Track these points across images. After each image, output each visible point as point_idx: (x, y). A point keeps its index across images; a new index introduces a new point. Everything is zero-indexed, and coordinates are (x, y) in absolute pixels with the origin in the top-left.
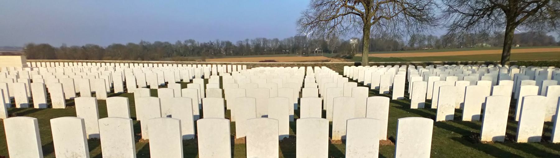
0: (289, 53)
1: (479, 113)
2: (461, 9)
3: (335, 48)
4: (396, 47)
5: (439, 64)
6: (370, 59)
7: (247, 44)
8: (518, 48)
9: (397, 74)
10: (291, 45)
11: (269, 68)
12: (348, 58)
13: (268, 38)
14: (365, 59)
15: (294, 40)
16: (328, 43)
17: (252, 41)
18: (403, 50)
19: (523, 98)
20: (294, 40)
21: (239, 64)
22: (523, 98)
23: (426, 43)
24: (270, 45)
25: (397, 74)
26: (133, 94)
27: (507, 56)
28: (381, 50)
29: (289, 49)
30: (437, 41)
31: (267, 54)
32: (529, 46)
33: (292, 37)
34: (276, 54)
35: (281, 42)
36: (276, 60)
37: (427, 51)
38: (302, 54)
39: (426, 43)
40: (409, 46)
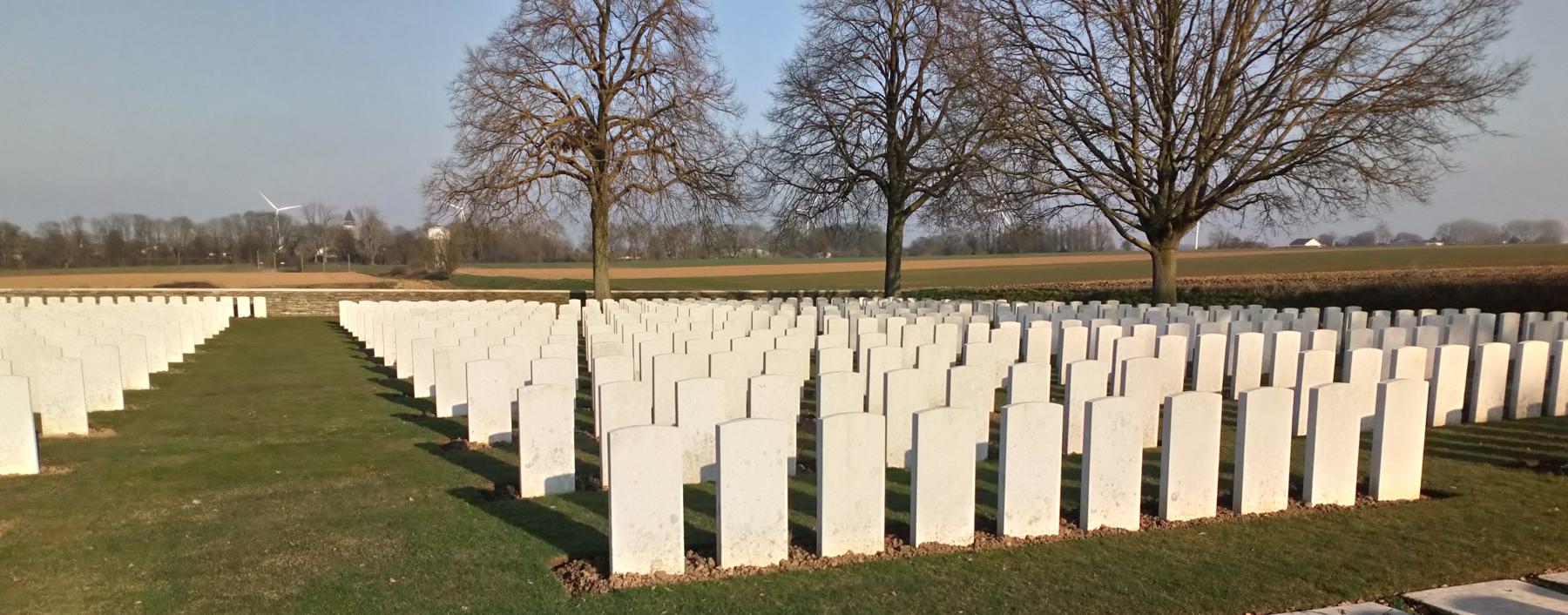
0: (230, 262)
1: (509, 429)
2: (796, 178)
3: (380, 249)
4: (554, 254)
5: (761, 295)
6: (615, 284)
7: (79, 235)
8: (828, 261)
9: (799, 313)
10: (235, 237)
11: (464, 303)
12: (432, 277)
13: (153, 214)
14: (603, 283)
15: (244, 222)
16: (357, 236)
17: (95, 222)
18: (569, 259)
19: (1069, 366)
20: (244, 222)
21: (243, 294)
22: (1069, 366)
23: (627, 244)
24: (163, 236)
25: (799, 313)
26: (151, 375)
27: (895, 279)
28: (512, 259)
29: (229, 249)
30: (653, 241)
31: (153, 263)
32: (798, 259)
33: (237, 216)
34: (184, 263)
35: (201, 229)
36: (214, 282)
37: (630, 264)
38: (278, 262)
39: (627, 244)
40: (584, 251)
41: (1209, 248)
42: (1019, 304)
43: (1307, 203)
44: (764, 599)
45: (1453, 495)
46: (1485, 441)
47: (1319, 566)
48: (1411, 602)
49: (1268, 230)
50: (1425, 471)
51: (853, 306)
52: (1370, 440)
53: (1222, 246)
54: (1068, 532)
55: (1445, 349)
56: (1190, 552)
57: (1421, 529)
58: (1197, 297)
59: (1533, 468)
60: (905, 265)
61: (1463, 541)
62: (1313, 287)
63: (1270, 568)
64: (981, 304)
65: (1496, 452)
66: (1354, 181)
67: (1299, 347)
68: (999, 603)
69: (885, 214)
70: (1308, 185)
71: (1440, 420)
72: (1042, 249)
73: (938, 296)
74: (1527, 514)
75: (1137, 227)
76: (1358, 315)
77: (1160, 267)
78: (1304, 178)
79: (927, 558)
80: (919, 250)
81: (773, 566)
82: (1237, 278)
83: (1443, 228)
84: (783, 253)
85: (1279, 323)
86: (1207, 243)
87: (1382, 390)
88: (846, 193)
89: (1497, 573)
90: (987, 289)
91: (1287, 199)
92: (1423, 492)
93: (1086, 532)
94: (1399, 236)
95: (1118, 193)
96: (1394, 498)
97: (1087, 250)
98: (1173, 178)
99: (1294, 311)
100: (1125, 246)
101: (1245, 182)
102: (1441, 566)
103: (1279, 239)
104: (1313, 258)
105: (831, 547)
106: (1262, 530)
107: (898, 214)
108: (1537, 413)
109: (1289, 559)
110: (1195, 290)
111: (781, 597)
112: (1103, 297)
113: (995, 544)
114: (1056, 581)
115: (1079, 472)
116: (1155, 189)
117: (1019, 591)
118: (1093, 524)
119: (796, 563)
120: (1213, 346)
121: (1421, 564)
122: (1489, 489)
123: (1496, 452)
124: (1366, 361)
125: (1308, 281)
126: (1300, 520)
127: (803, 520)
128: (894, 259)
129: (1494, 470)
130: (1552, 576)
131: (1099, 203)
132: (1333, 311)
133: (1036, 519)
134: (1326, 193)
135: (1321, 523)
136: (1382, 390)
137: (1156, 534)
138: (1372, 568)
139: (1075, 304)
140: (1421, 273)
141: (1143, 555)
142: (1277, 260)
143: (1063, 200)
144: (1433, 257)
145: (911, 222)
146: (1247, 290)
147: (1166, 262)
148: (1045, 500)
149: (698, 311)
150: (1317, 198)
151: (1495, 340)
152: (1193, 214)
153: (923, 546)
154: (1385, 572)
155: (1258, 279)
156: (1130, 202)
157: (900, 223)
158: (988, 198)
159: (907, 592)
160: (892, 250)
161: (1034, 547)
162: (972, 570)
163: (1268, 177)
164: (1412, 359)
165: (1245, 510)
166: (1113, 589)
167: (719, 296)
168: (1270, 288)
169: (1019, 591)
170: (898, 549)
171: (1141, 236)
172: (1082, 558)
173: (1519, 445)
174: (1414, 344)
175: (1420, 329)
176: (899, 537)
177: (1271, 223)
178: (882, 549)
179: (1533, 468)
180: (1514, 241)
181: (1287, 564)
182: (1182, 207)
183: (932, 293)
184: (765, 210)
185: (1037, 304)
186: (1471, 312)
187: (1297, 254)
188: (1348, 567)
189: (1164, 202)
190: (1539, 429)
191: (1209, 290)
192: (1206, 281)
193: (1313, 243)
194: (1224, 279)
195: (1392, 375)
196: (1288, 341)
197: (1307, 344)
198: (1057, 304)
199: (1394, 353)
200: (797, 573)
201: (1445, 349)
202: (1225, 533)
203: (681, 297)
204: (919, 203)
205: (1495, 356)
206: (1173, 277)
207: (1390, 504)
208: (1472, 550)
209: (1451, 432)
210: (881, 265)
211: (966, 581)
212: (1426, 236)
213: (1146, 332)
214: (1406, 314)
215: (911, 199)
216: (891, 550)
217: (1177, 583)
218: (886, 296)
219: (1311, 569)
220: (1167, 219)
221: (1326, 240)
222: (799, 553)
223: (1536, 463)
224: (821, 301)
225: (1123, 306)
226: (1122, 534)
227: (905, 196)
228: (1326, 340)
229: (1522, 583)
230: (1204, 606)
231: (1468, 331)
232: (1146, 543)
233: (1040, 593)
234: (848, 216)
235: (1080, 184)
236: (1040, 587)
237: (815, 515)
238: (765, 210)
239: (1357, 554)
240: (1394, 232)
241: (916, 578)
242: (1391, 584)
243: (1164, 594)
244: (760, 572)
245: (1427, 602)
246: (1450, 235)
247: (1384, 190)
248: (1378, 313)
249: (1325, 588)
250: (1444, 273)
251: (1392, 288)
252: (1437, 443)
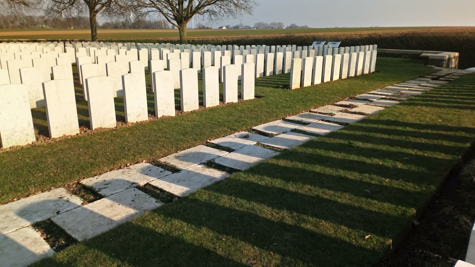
8: (72, 30)
41: (197, 29)
42: (138, 44)
43: (221, 13)
44: (21, 160)
45: (263, 97)
46: (269, 81)
47: (229, 122)
48: (254, 130)
49: (211, 22)
50: (255, 91)
51: (78, 45)
52: (240, 83)
53: (200, 28)
54: (152, 119)
55: (258, 55)
56: (190, 121)
57: (255, 107)
58: (194, 43)
59: (282, 88)
60: (99, 32)
61: (266, 110)
62: (225, 40)
63: (214, 124)
64: (125, 44)
65: (272, 84)
66: (233, 7)
67: (222, 56)
68: (124, 148)
69: (88, 12)
70: (221, 7)
71: (258, 76)
72: (147, 27)
73: (111, 41)
74: (281, 101)
75: (173, 19)
76: (236, 47)
77: (182, 33)
78: (220, 5)
79: (97, 134)
80: (105, 26)
81: (29, 144)
82: (204, 38)
83: (256, 24)
84: (54, 27)
85: (216, 49)
86: (196, 27)
87: (243, 66)
88: (73, 4)
89: (275, 119)
90: (129, 40)
91: (215, 12)
92: (255, 96)
93: (158, 118)
94: (246, 26)
95: (166, 7)
96: (248, 99)
97: (161, 28)
98: (182, 4)
99: (220, 46)
100: (172, 26)
101: (204, 6)
102: (261, 118)
103: (215, 26)
104: (224, 32)
105: (56, 133)
106: (212, 112)
107: (93, 12)
108: (281, 73)
109: (220, 120)
110: (193, 41)
111: (29, 158)
112: (166, 42)
113: (124, 126)
114: (145, 137)
115: (153, 98)
116: (177, 7)
117: (131, 142)
118: (160, 115)
119: (40, 142)
120: (197, 55)
121: (256, 118)
122: (271, 94)
123: (272, 84)
124: (238, 59)
125: (223, 38)
126: (223, 108)
127: (121, 113)
128: (94, 28)
129: (272, 89)
130: (288, 118)
131: (161, 11)
132: (230, 46)
133: (139, 115)
134: (226, 10)
135: (229, 108)
136: (243, 66)
137: (180, 117)
138: (243, 121)
139: (157, 44)
140: (252, 36)
141: (176, 124)
142: (214, 33)
143: (149, 9)
144: (253, 32)
145: (98, 15)
146: (207, 41)
147: (183, 31)
148: (142, 108)
149: (13, 47)
150: (223, 12)
151: (270, 52)
152: (189, 15)
153: (96, 129)
154: (246, 122)
155: (210, 38)
156: (170, 11)
157: (95, 15)
158: (123, 7)
159: (87, 148)
160: (93, 24)
161: (139, 125)
162: (114, 137)
163: (210, 5)
164: (250, 58)
165: (207, 106)
166: (165, 137)
167: (25, 41)
168: (213, 40)
169: (131, 142)
170: (86, 131)
171: (175, 22)
172: (155, 128)
173: (277, 82)
174: (250, 54)
175: (252, 50)
176: (86, 127)
177: (212, 19)
178: (79, 132)
179: (282, 88)
180: (272, 28)
181: (219, 122)
182: (186, 13)
183: (109, 40)
184: (40, 9)
185: (145, 44)
186: (264, 46)
187: (220, 31)
188: (236, 121)
189: (180, 11)
190: (282, 77)
191: (197, 41)
192: (196, 38)
193: (224, 28)
194: (201, 38)
195: (245, 62)
196: (218, 54)
197: (223, 54)
198: (151, 44)
199: (246, 56)
200: (39, 146)
201: (258, 55)
202: (201, 114)
203: (8, 42)
204: (101, 8)
205: (271, 56)
206: (185, 37)
207: (247, 101)
208: (268, 112)
209: (261, 79)
210: (89, 32)
211: (112, 141)
212: (252, 27)
213: (177, 51)
214: (248, 46)
215: (98, 7)
216: (83, 132)
217: (186, 133)
218: (93, 41)
219: (226, 123)
220: (182, 17)
221: (227, 27)
222: (41, 138)
223: (282, 86)
224: (68, 44)
225: (172, 45)
226: (170, 118)
227: (95, 6)
228: (228, 54)
229: (281, 121)
230: (194, 140)
231: (264, 51)
232: (177, 120)
233: (139, 142)
234: (74, 13)
235: (154, 4)
236: (140, 140)
237: (124, 111)
238: (40, 9)
239: (239, 117)
240: (244, 25)
241: (91, 142)
242: (248, 125)
243: (182, 137)
244: (22, 148)
245: (258, 129)
246: (258, 26)
247: (241, 10)
248: (241, 46)
249: (230, 129)
250: (257, 36)
251: (245, 40)
252: (258, 83)
